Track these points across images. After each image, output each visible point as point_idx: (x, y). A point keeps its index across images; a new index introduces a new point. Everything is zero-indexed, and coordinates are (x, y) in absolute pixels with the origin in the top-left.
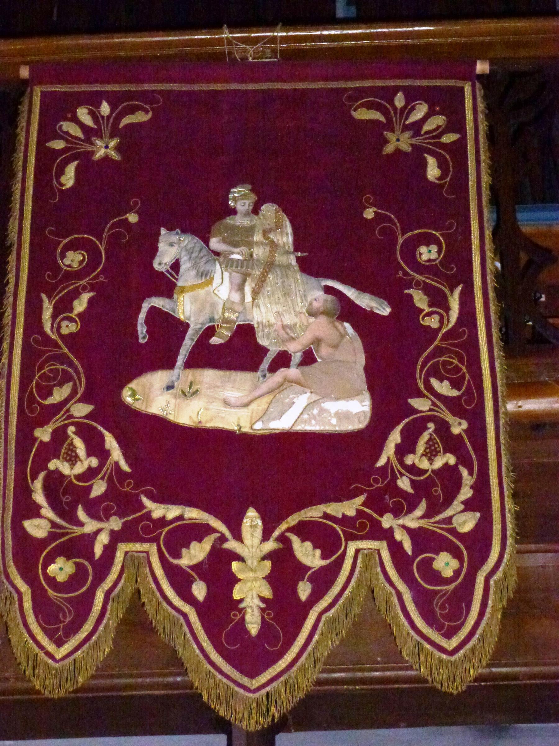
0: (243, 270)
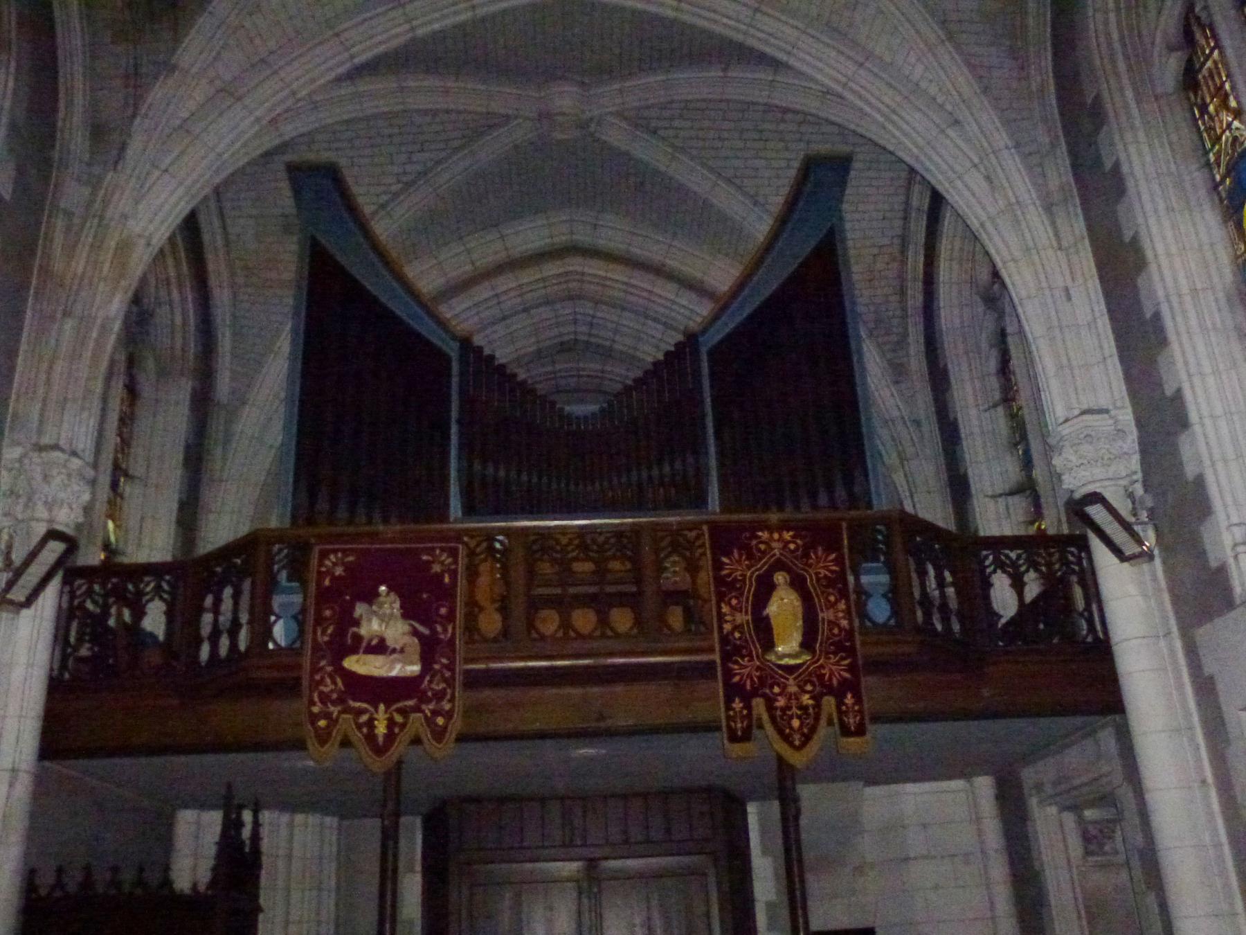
0: (382, 619)
